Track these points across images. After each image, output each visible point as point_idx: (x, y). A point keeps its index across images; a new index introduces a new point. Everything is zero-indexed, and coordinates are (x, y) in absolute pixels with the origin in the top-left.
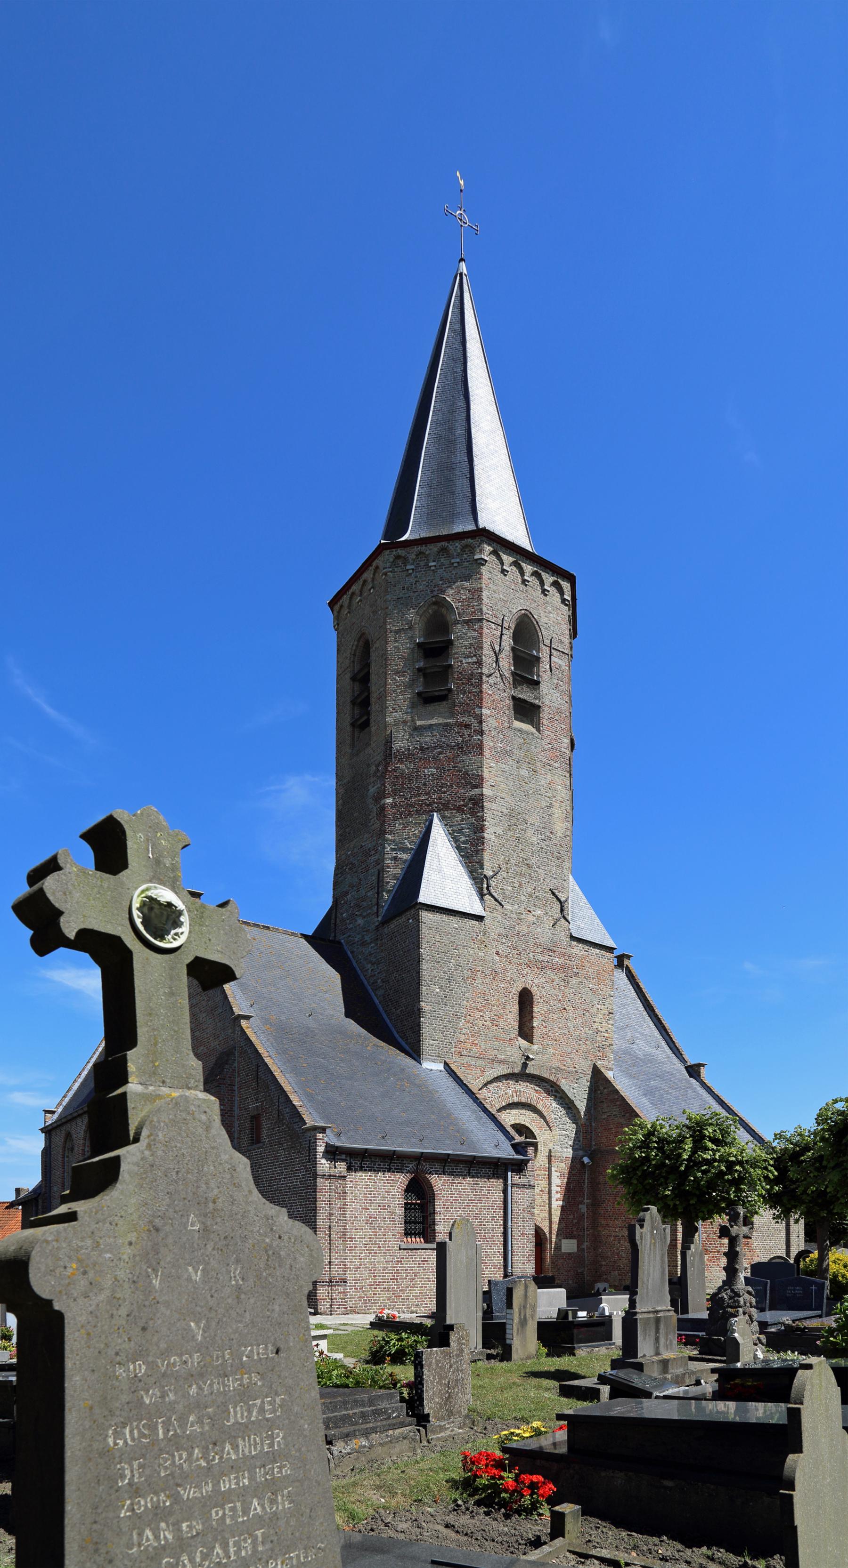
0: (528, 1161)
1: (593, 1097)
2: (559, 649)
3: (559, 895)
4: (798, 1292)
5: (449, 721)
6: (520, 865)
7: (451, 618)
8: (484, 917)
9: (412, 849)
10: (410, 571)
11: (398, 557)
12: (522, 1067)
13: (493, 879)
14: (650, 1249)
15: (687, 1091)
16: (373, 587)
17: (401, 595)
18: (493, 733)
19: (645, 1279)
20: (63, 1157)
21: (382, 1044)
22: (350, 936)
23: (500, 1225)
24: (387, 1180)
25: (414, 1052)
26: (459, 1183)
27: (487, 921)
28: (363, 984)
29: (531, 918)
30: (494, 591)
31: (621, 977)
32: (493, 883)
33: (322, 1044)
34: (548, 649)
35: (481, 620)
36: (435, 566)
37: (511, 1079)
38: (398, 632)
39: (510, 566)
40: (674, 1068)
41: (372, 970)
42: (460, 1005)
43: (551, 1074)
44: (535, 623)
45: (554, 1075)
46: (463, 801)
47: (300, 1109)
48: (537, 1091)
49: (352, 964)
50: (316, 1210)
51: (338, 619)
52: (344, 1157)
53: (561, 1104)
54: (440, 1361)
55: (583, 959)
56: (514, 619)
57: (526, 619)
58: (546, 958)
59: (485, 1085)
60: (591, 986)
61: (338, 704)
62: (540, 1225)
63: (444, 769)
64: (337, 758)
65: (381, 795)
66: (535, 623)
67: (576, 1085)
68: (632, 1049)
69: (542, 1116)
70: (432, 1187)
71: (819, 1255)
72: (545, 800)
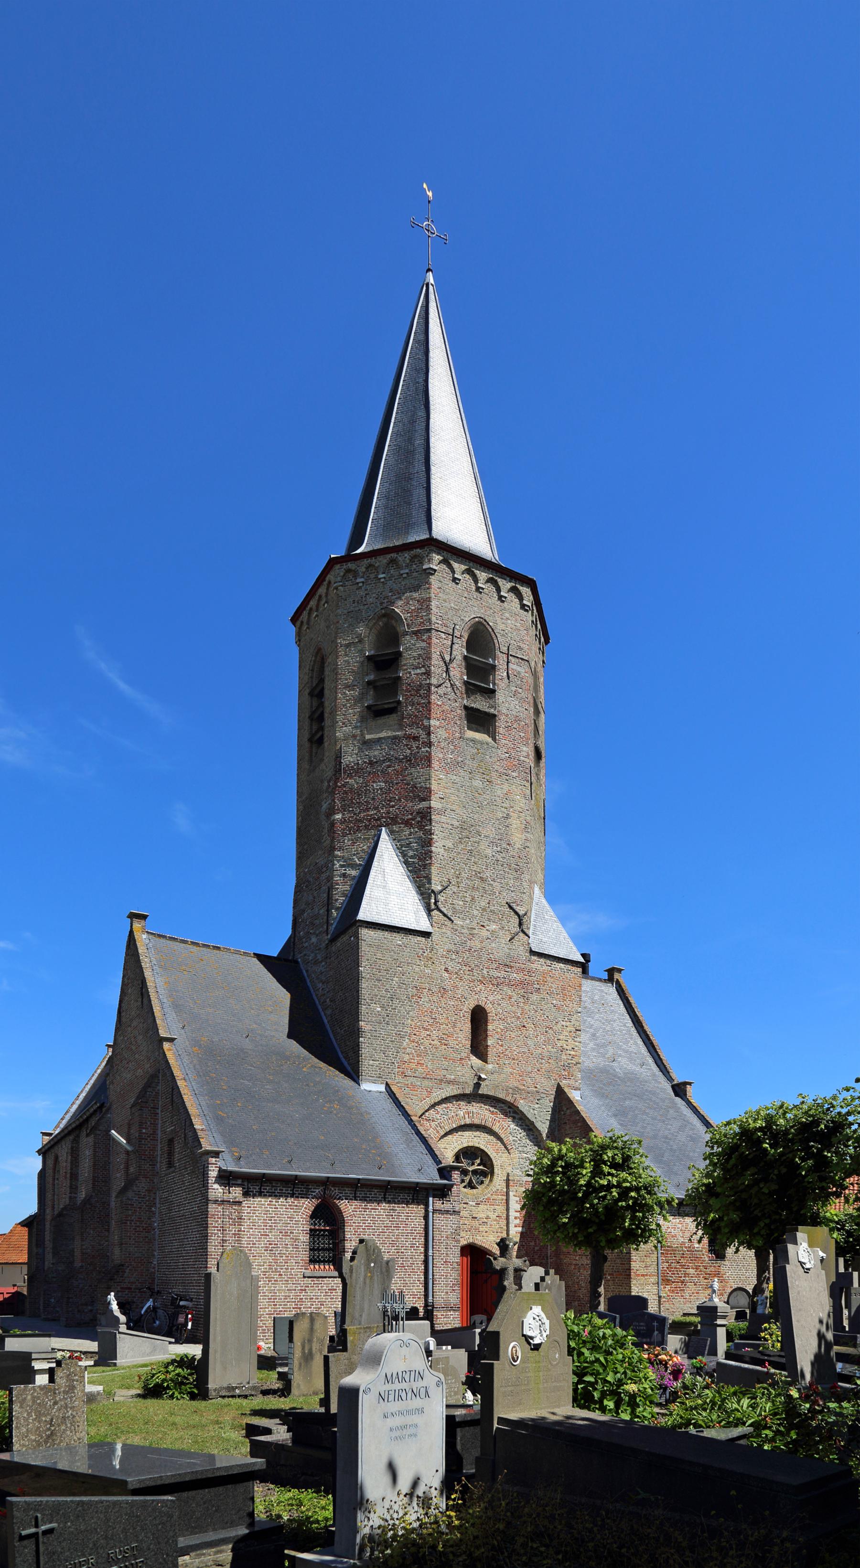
0: (452, 1186)
1: (557, 1117)
2: (517, 655)
3: (517, 909)
4: (642, 1328)
5: (397, 733)
6: (472, 878)
7: (400, 629)
8: (431, 933)
9: (360, 865)
10: (361, 585)
11: (348, 571)
12: (474, 1088)
13: (442, 894)
14: (365, 1283)
15: (668, 1111)
16: (326, 602)
17: (352, 609)
18: (442, 744)
19: (357, 1315)
20: (54, 1180)
21: (322, 1065)
22: (305, 955)
23: (421, 1253)
25: (353, 1073)
27: (434, 937)
28: (315, 1004)
29: (484, 933)
31: (612, 990)
33: (252, 1066)
34: (505, 656)
35: (429, 630)
36: (384, 578)
37: (463, 1100)
38: (348, 646)
39: (463, 573)
40: (658, 1087)
41: (323, 989)
42: (403, 1024)
43: (507, 1094)
44: (490, 630)
45: (510, 1095)
46: (411, 814)
47: (200, 1133)
48: (492, 1113)
49: (306, 982)
50: (207, 1236)
51: (299, 634)
52: (239, 1182)
53: (520, 1126)
54: (38, 1398)
55: (544, 974)
56: (467, 628)
57: (482, 627)
58: (502, 974)
59: (433, 1106)
60: (554, 1002)
61: (299, 721)
63: (392, 782)
64: (298, 775)
65: (332, 811)
66: (490, 630)
67: (537, 1106)
68: (612, 1067)
69: (499, 1138)
70: (342, 1213)
71: (774, 1287)
72: (501, 811)
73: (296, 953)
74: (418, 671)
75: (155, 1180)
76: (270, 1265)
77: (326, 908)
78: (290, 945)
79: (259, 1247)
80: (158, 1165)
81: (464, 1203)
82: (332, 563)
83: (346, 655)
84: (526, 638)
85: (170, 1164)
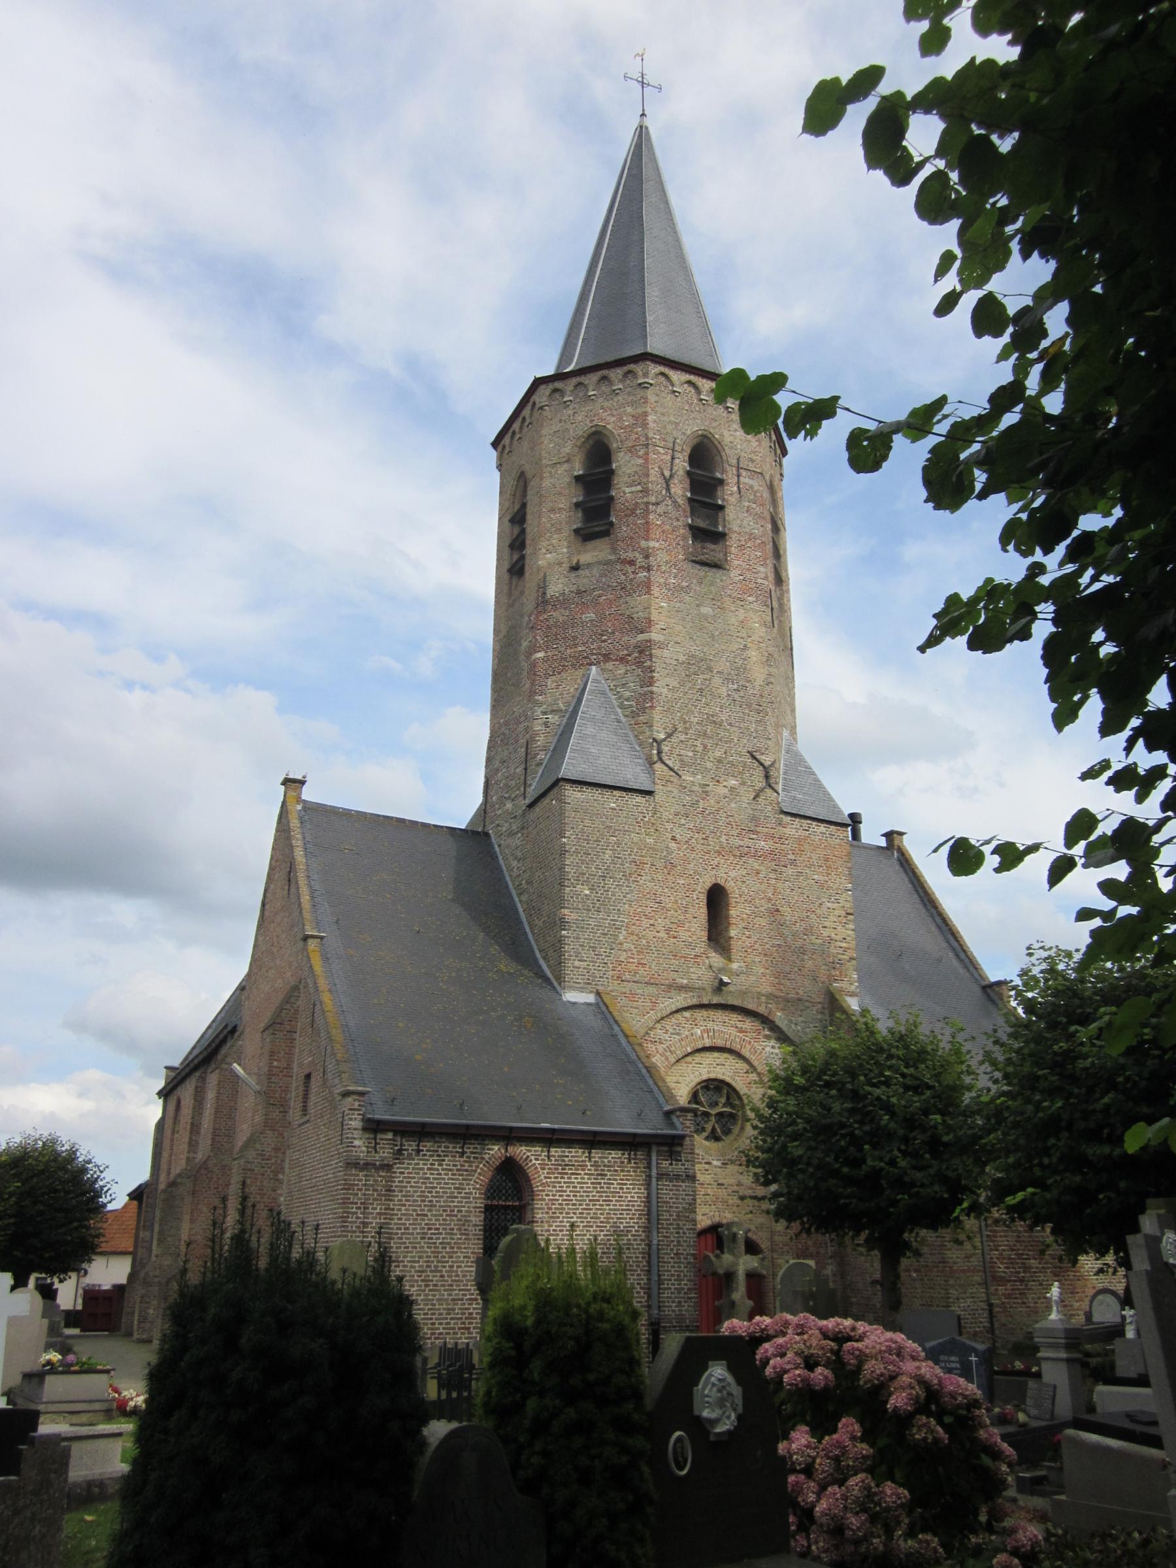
3: (762, 758)
11: (556, 390)
22: (498, 825)
24: (458, 1170)
26: (572, 1174)
30: (663, 414)
32: (665, 748)
42: (619, 910)
43: (759, 1005)
55: (800, 841)
58: (747, 842)
60: (816, 877)
62: (754, 1237)
65: (533, 649)
70: (530, 1181)
73: (487, 823)
74: (634, 489)
75: (285, 1134)
76: (428, 1261)
77: (523, 766)
78: (484, 811)
79: (413, 1234)
80: (291, 1111)
81: (706, 1163)
82: (538, 383)
83: (551, 476)
84: (758, 449)
85: (305, 1110)
